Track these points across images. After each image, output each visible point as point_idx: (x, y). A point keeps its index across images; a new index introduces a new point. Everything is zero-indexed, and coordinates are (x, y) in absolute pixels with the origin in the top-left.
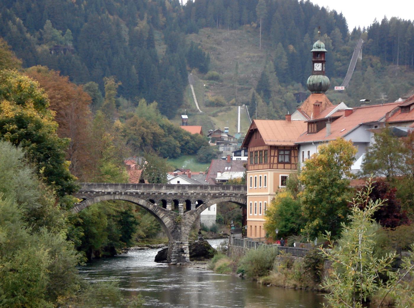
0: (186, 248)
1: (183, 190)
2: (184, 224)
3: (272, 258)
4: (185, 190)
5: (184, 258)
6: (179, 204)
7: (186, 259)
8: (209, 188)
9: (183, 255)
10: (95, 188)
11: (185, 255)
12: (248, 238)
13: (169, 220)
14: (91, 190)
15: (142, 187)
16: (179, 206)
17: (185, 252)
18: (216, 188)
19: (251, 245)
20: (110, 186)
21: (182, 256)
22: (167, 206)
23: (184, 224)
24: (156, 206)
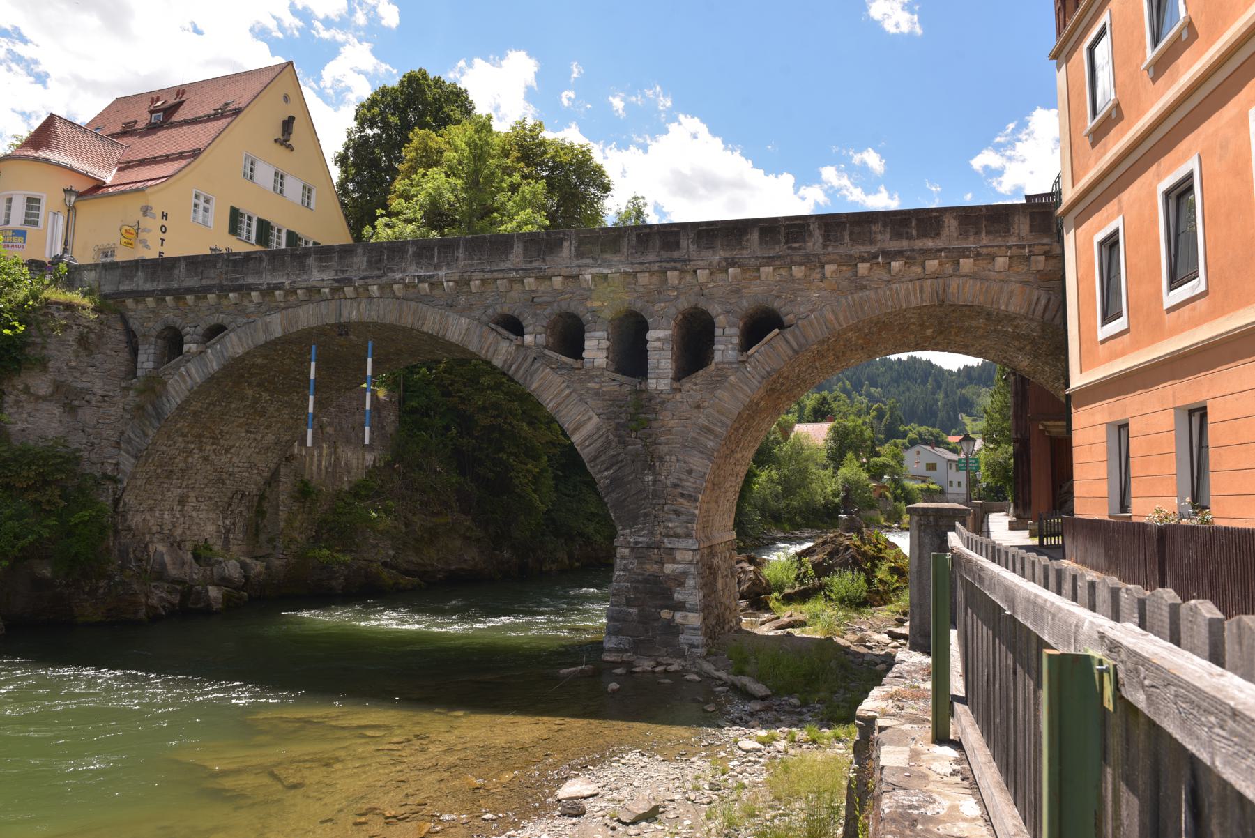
0: (685, 574)
1: (666, 255)
2: (492, 751)
3: (479, 347)
4: (676, 255)
5: (673, 629)
6: (651, 335)
7: (682, 638)
8: (811, 235)
9: (665, 614)
10: (258, 273)
11: (678, 616)
12: (48, 286)
13: (596, 419)
14: (241, 282)
15: (460, 253)
16: (650, 345)
17: (678, 597)
18: (857, 229)
19: (30, 218)
20: (321, 260)
21: (659, 618)
22: (587, 344)
23: (492, 751)
24: (529, 347)
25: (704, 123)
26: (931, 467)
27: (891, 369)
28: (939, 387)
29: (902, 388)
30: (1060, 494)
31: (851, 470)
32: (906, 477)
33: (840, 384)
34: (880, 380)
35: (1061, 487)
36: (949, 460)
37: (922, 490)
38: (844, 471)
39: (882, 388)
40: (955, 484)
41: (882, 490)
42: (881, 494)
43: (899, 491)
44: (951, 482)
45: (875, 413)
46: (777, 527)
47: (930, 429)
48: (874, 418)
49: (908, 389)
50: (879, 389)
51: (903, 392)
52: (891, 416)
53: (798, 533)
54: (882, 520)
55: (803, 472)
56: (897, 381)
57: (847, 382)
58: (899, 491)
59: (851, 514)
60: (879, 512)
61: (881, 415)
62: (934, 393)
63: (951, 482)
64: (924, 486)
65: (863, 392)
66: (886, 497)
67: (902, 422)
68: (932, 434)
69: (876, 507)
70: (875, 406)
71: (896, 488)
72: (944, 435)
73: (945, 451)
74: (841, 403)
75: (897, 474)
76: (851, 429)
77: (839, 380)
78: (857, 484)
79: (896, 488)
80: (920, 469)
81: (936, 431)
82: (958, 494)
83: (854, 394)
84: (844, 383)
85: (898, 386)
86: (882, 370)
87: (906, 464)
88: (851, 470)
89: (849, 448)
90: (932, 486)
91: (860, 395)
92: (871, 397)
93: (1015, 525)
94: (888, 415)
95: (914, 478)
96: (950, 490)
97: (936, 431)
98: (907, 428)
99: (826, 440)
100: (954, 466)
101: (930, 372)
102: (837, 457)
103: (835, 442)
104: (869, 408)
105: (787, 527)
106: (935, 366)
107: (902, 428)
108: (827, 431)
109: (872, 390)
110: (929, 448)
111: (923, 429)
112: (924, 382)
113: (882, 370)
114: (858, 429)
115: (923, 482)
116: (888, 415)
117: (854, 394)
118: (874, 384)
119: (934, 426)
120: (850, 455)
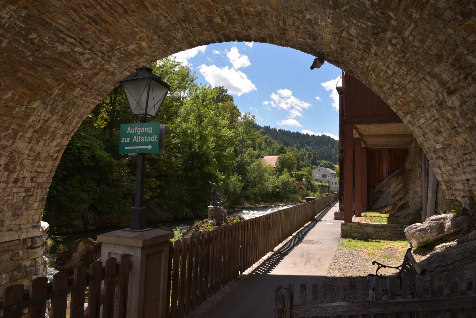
25: (284, 89)
26: (325, 176)
27: (315, 139)
28: (333, 146)
29: (319, 147)
30: (373, 193)
31: (285, 177)
32: (313, 180)
33: (296, 144)
34: (311, 143)
35: (374, 187)
36: (332, 173)
37: (320, 186)
38: (282, 177)
39: (312, 146)
40: (334, 183)
41: (301, 186)
42: (300, 187)
43: (309, 186)
44: (332, 182)
45: (307, 155)
46: (248, 202)
47: (328, 162)
48: (307, 157)
49: (322, 147)
50: (311, 147)
51: (320, 148)
52: (314, 157)
53: (257, 205)
54: (300, 198)
55: (261, 176)
56: (317, 144)
57: (299, 144)
58: (309, 186)
59: (217, 205)
60: (299, 195)
61: (310, 157)
62: (331, 149)
63: (332, 182)
64: (321, 184)
65: (305, 148)
66: (303, 189)
67: (318, 159)
68: (329, 164)
69: (297, 193)
70: (308, 153)
71: (308, 185)
72: (334, 165)
73: (330, 170)
74: (295, 151)
75: (309, 179)
76: (287, 158)
77: (295, 143)
78: (288, 182)
79: (308, 185)
80: (320, 177)
81: (330, 163)
82: (335, 187)
83: (301, 148)
84: (297, 144)
85: (318, 146)
86: (312, 139)
87: (313, 174)
88: (285, 177)
89: (286, 166)
90: (324, 184)
91: (304, 149)
92: (308, 150)
93: (339, 216)
94: (312, 156)
95: (317, 180)
96: (332, 186)
97: (330, 163)
98: (320, 161)
99: (276, 163)
100: (334, 176)
101: (330, 141)
102: (280, 170)
103: (280, 164)
104: (305, 153)
105: (253, 202)
106: (332, 138)
107: (318, 161)
108: (277, 159)
109: (308, 147)
110: (324, 168)
111: (326, 162)
112: (328, 145)
113: (312, 139)
114: (290, 159)
115: (321, 182)
116: (312, 156)
117: (301, 148)
118: (309, 145)
119: (330, 161)
120: (285, 170)
